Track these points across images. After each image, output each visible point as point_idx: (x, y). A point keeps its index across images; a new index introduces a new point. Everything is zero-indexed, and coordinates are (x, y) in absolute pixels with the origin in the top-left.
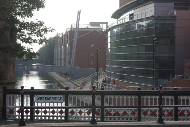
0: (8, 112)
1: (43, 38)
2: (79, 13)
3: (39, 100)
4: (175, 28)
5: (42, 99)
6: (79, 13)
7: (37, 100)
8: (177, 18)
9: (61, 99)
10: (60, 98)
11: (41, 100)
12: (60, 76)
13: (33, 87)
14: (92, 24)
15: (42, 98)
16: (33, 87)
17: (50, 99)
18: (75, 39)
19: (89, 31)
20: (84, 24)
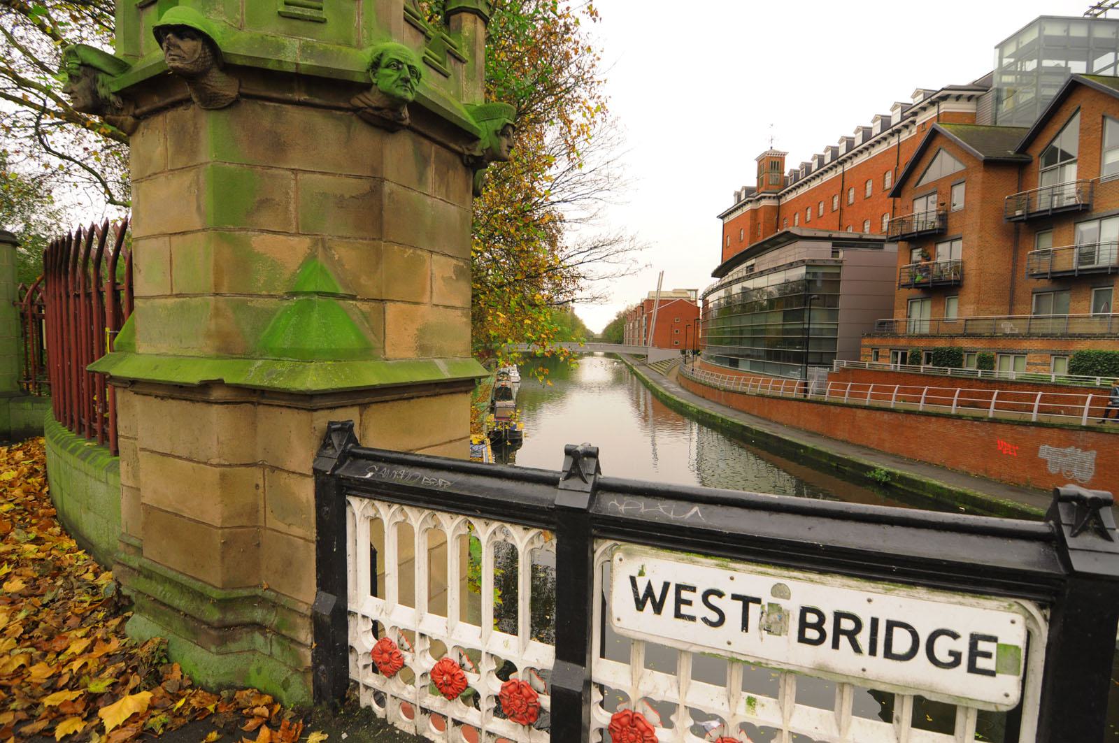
0: (360, 650)
1: (1072, 356)
2: (662, 274)
3: (658, 608)
4: (983, 182)
5: (698, 609)
6: (662, 274)
7: (640, 605)
8: (844, 263)
9: (974, 653)
10: (963, 646)
11: (678, 615)
12: (481, 484)
13: (593, 454)
14: (675, 291)
15: (696, 598)
16: (593, 454)
17: (803, 625)
18: (655, 311)
19: (668, 301)
20: (668, 288)
